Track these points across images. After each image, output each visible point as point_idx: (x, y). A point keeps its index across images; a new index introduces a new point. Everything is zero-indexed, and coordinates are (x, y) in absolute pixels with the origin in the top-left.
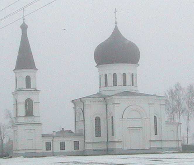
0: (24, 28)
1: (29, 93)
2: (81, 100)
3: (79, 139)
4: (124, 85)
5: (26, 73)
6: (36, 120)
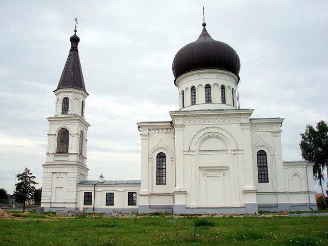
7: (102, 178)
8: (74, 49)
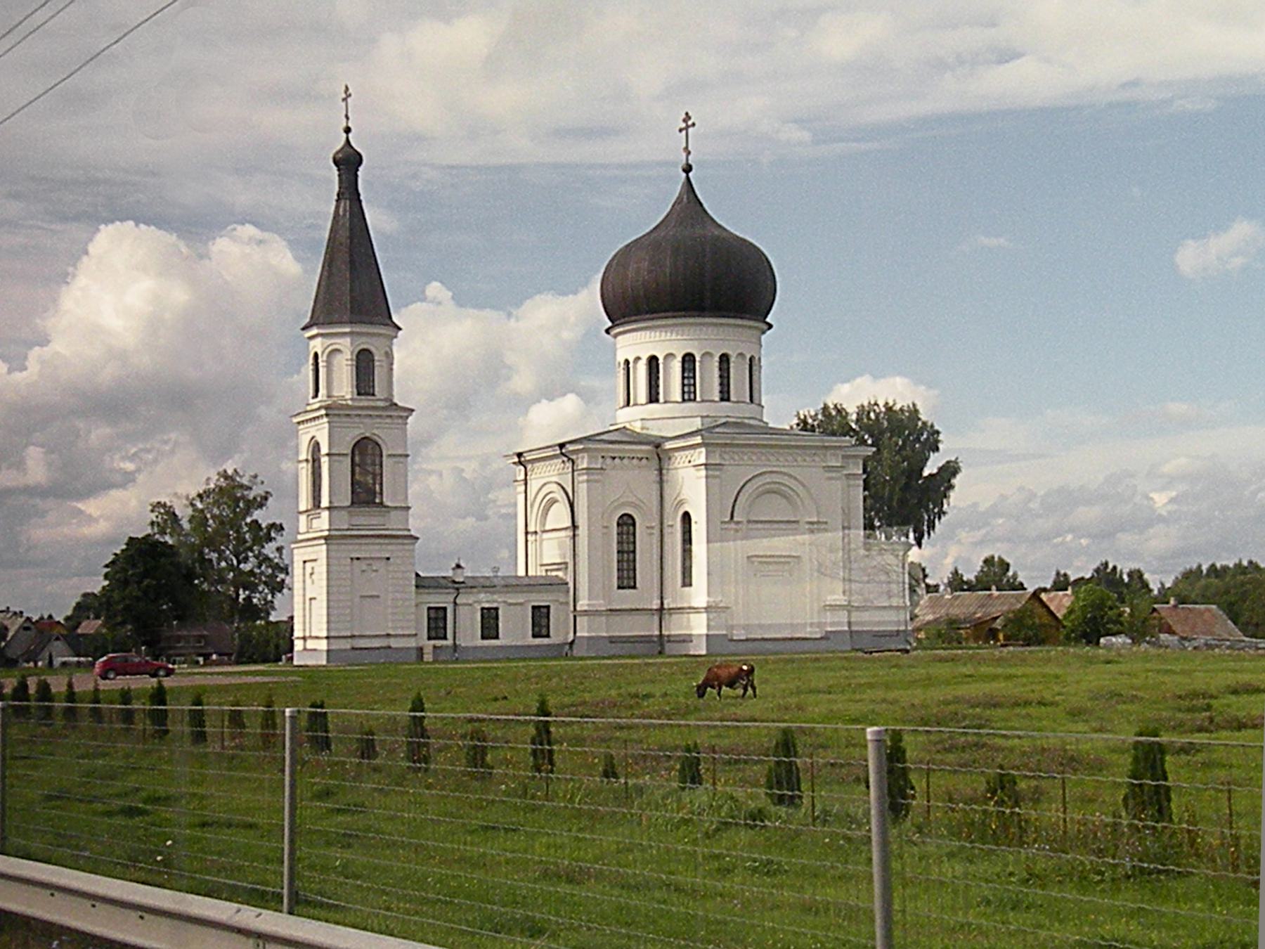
4: (722, 399)
6: (393, 523)
7: (459, 571)
8: (349, 192)
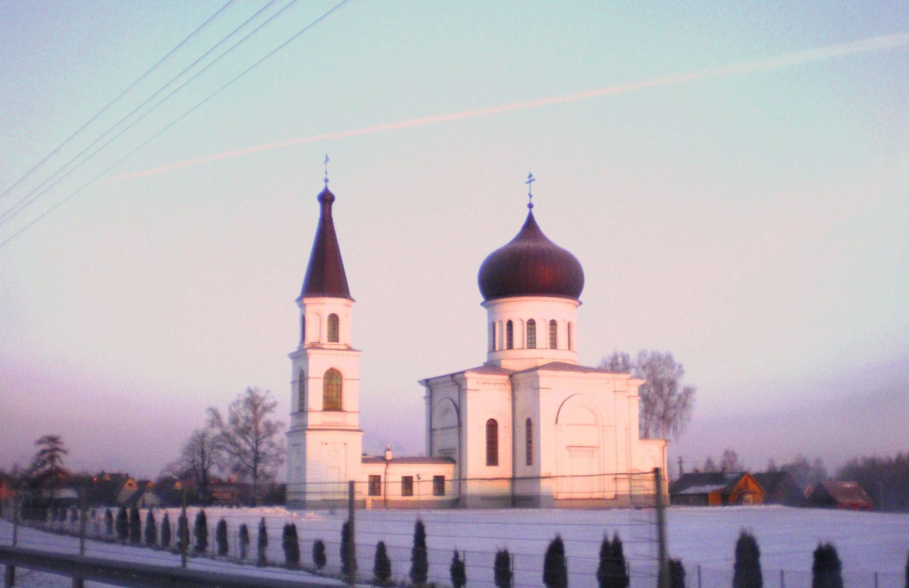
0: (326, 199)
1: (336, 355)
2: (454, 378)
3: (446, 470)
5: (330, 305)
